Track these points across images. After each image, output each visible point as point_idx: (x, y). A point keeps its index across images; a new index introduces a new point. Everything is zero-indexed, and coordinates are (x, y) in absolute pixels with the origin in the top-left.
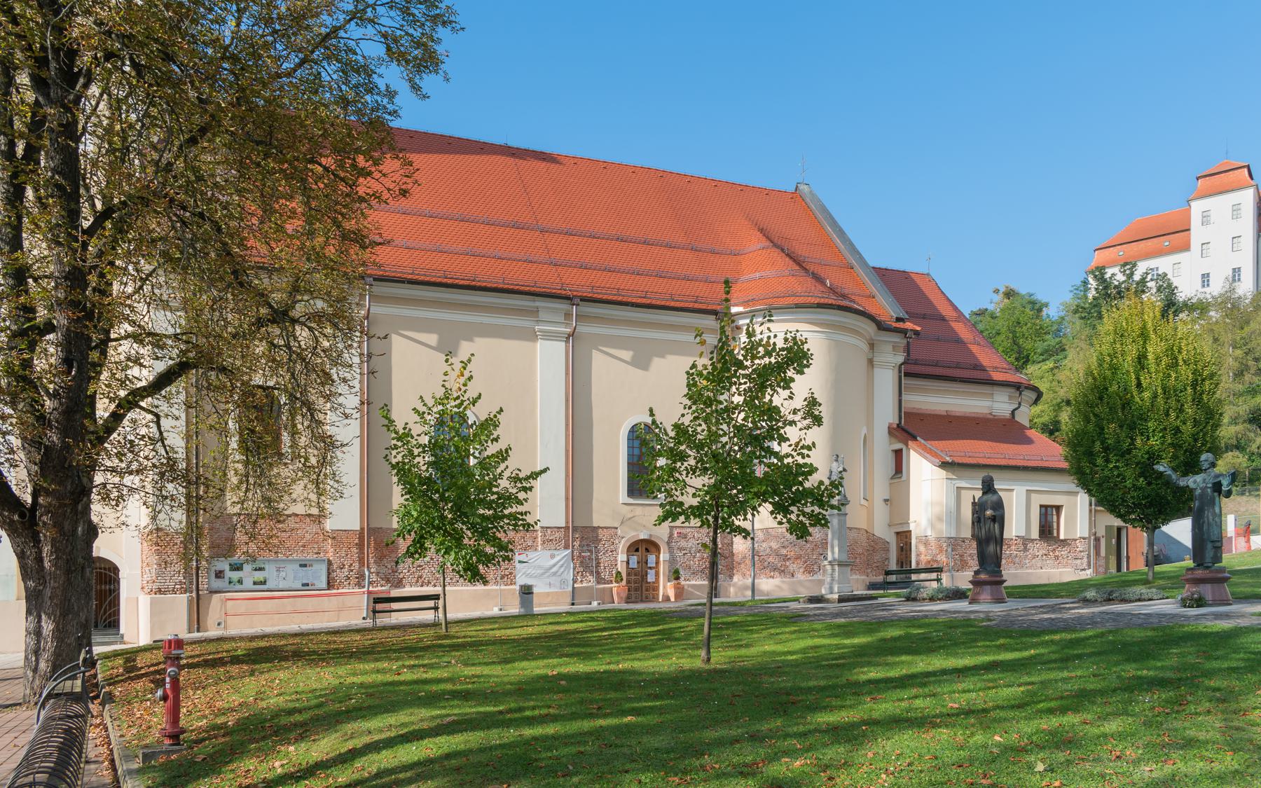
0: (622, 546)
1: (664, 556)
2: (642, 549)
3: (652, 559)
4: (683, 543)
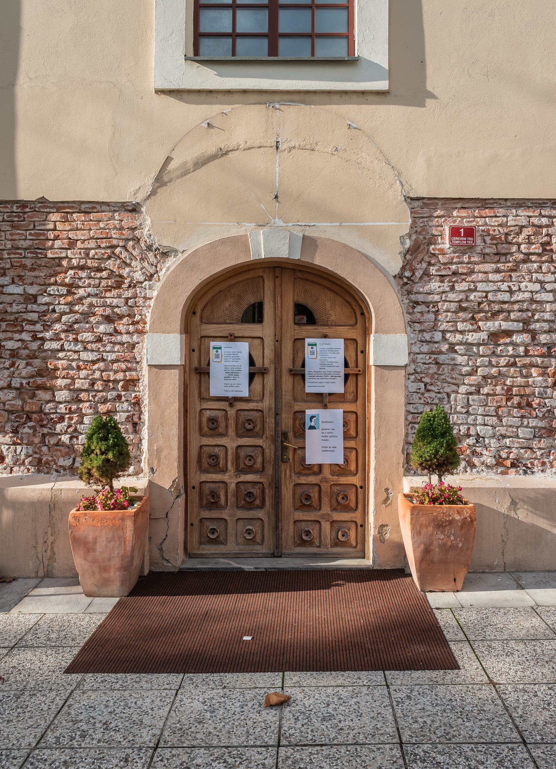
0: (163, 293)
1: (389, 346)
2: (278, 304)
3: (324, 356)
4: (487, 280)
